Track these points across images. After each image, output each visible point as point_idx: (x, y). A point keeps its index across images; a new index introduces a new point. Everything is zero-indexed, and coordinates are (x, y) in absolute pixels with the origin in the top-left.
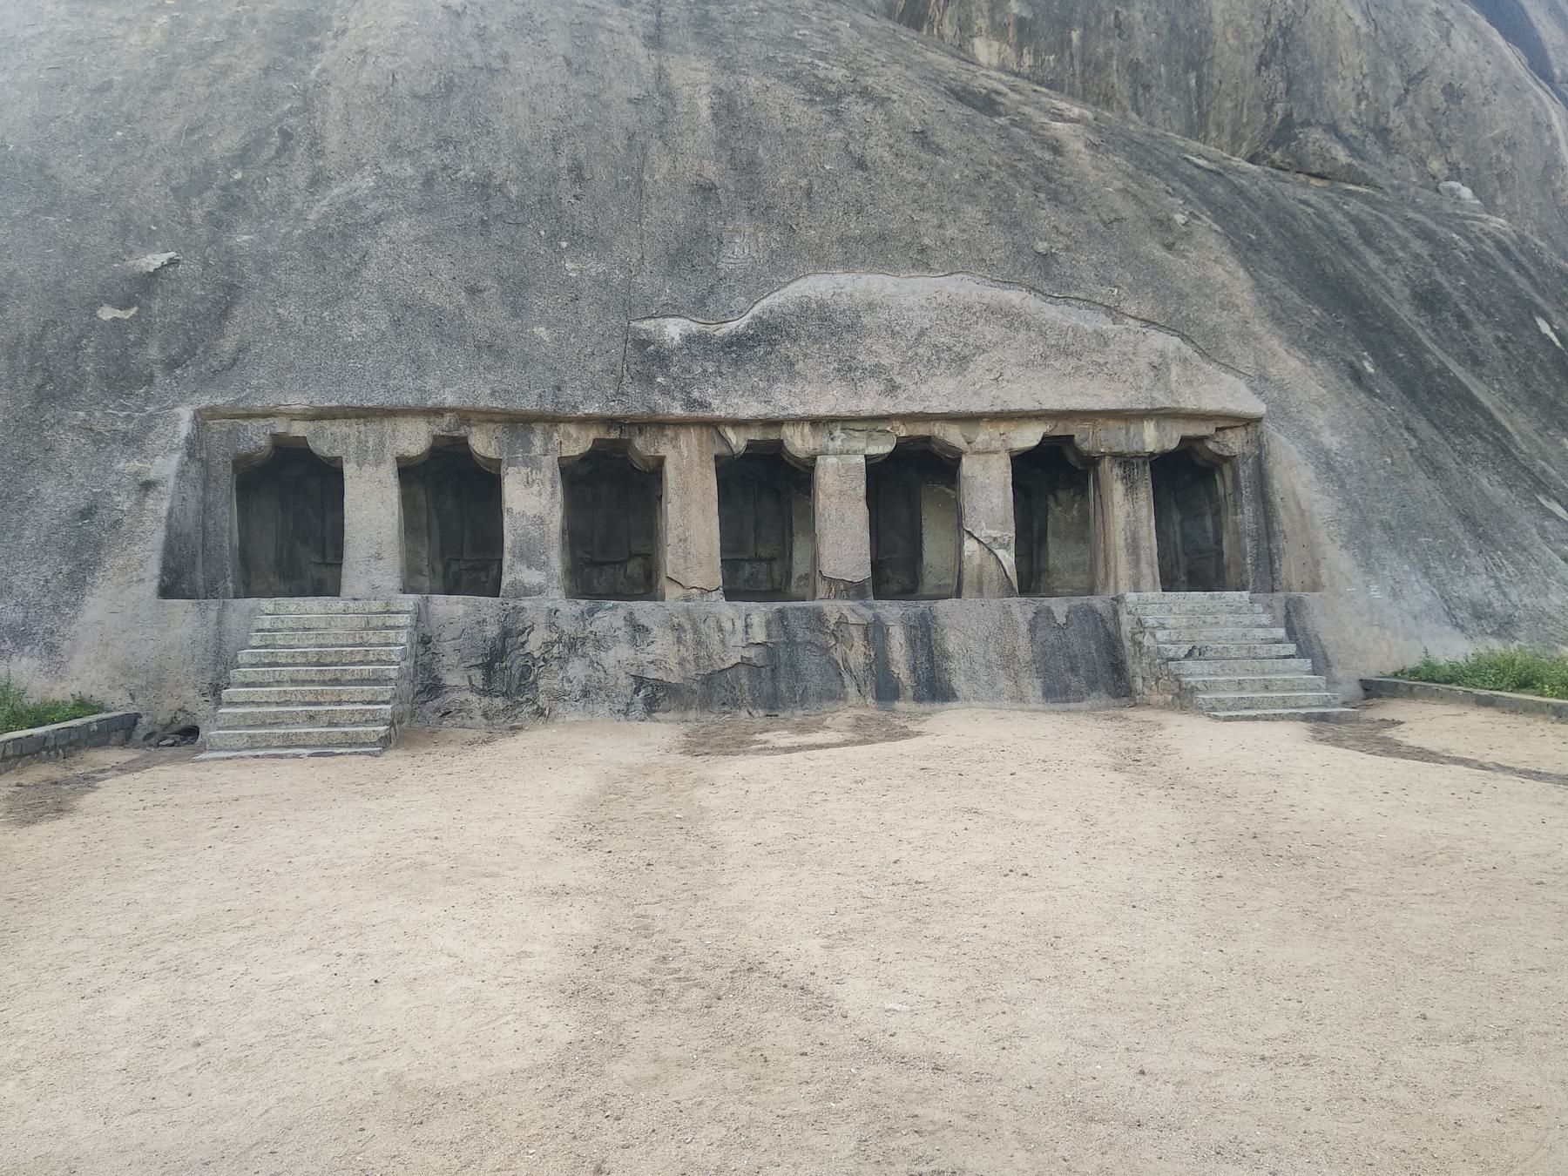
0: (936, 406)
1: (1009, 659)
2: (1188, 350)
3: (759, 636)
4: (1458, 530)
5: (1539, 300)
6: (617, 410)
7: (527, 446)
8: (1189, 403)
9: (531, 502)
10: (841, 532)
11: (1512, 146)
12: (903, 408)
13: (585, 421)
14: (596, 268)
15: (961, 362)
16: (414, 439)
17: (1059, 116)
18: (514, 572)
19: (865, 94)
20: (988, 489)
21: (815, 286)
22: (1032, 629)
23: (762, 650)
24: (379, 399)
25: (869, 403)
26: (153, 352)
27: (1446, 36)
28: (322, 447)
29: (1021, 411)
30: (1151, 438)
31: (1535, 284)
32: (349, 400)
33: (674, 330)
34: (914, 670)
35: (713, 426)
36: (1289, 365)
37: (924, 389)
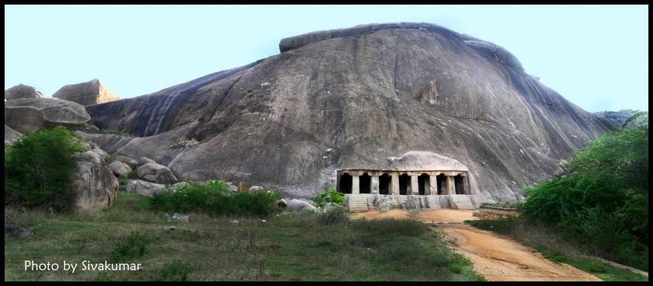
4: (495, 186)
5: (521, 146)
9: (375, 182)
10: (415, 186)
11: (521, 117)
13: (382, 171)
14: (382, 150)
15: (430, 164)
16: (361, 173)
17: (443, 126)
18: (373, 191)
19: (416, 124)
20: (433, 181)
24: (358, 168)
27: (509, 97)
28: (350, 174)
30: (454, 174)
31: (521, 143)
32: (354, 168)
33: (393, 159)
36: (472, 164)
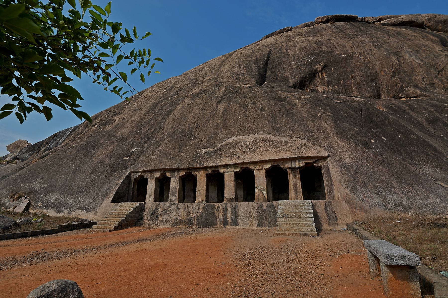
0: (246, 161)
1: (251, 216)
2: (308, 143)
3: (201, 210)
6: (187, 166)
7: (175, 174)
8: (305, 155)
12: (240, 161)
21: (231, 140)
22: (258, 209)
23: (201, 213)
25: (234, 161)
26: (130, 163)
28: (145, 177)
29: (264, 160)
34: (231, 219)
35: (206, 168)
37: (245, 157)
